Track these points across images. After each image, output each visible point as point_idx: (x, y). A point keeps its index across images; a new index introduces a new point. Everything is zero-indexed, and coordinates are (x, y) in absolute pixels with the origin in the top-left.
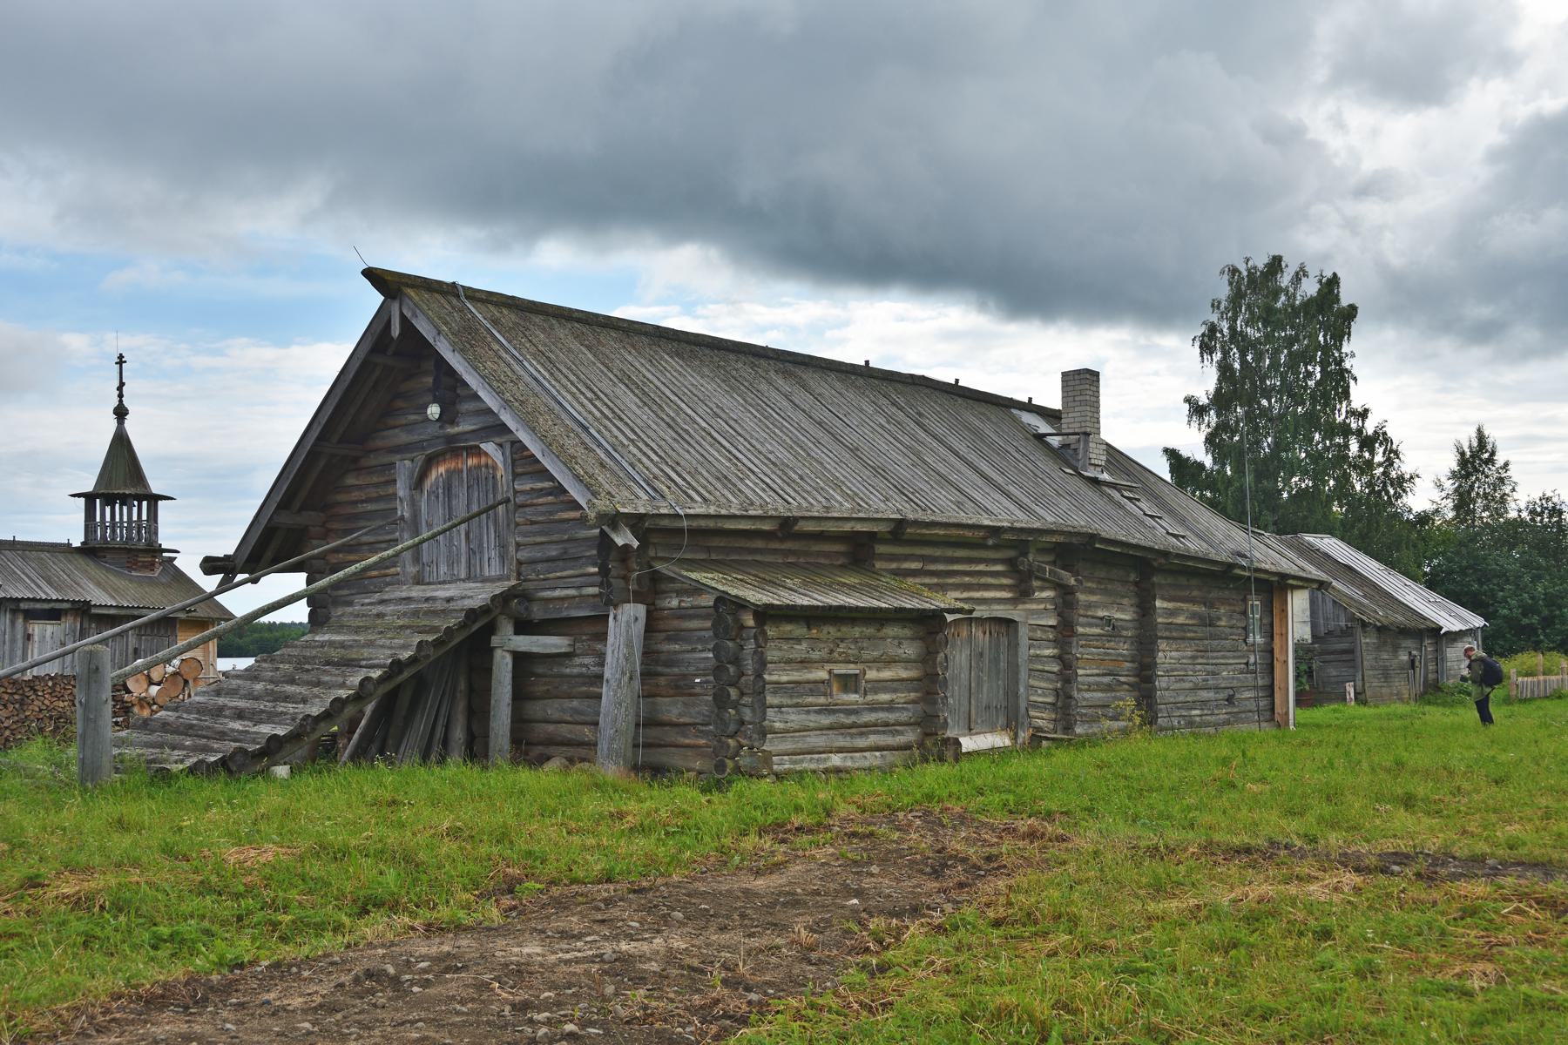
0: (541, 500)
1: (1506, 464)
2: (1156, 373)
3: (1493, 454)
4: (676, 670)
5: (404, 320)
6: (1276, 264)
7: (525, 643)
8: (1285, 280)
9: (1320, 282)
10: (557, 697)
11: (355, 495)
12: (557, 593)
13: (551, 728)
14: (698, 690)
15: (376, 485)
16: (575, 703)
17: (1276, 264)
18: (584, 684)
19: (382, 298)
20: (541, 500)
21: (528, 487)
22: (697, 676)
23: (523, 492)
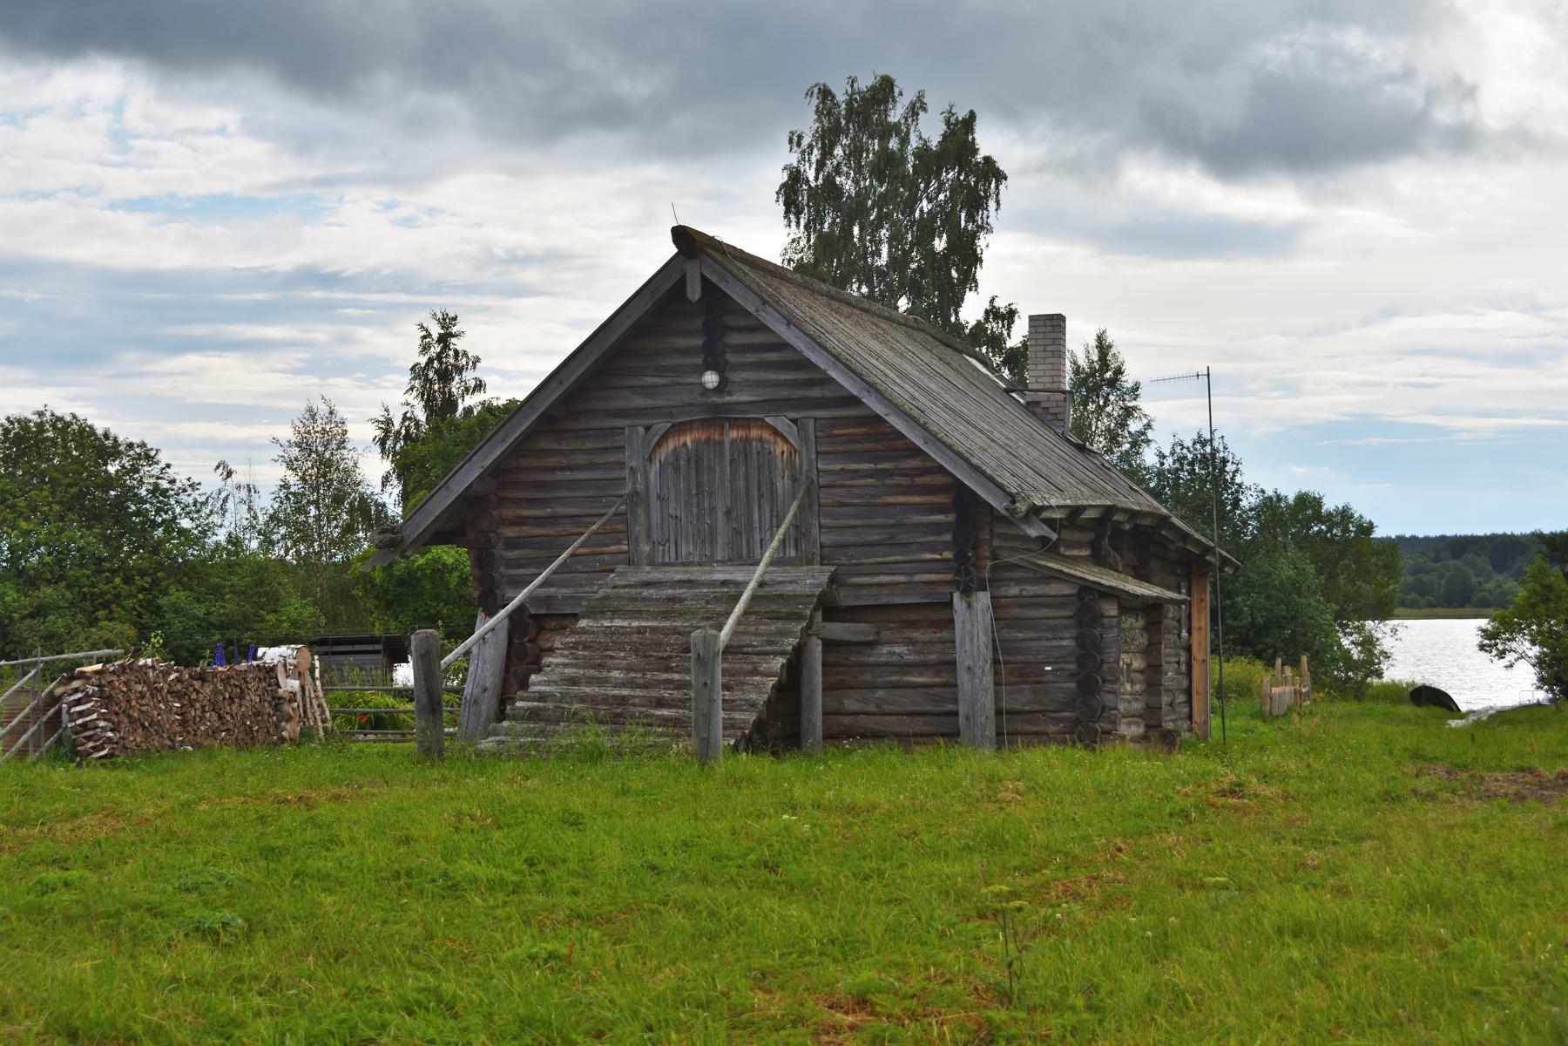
0: (856, 482)
1: (1136, 388)
2: (222, 131)
3: (1119, 371)
4: (1021, 658)
5: (706, 283)
6: (884, 90)
7: (837, 630)
8: (895, 115)
9: (948, 122)
10: (852, 687)
11: (552, 461)
12: (867, 580)
13: (847, 720)
14: (1048, 677)
15: (588, 452)
16: (880, 693)
17: (884, 90)
18: (895, 673)
19: (676, 250)
20: (856, 482)
21: (839, 467)
22: (1048, 664)
23: (827, 472)
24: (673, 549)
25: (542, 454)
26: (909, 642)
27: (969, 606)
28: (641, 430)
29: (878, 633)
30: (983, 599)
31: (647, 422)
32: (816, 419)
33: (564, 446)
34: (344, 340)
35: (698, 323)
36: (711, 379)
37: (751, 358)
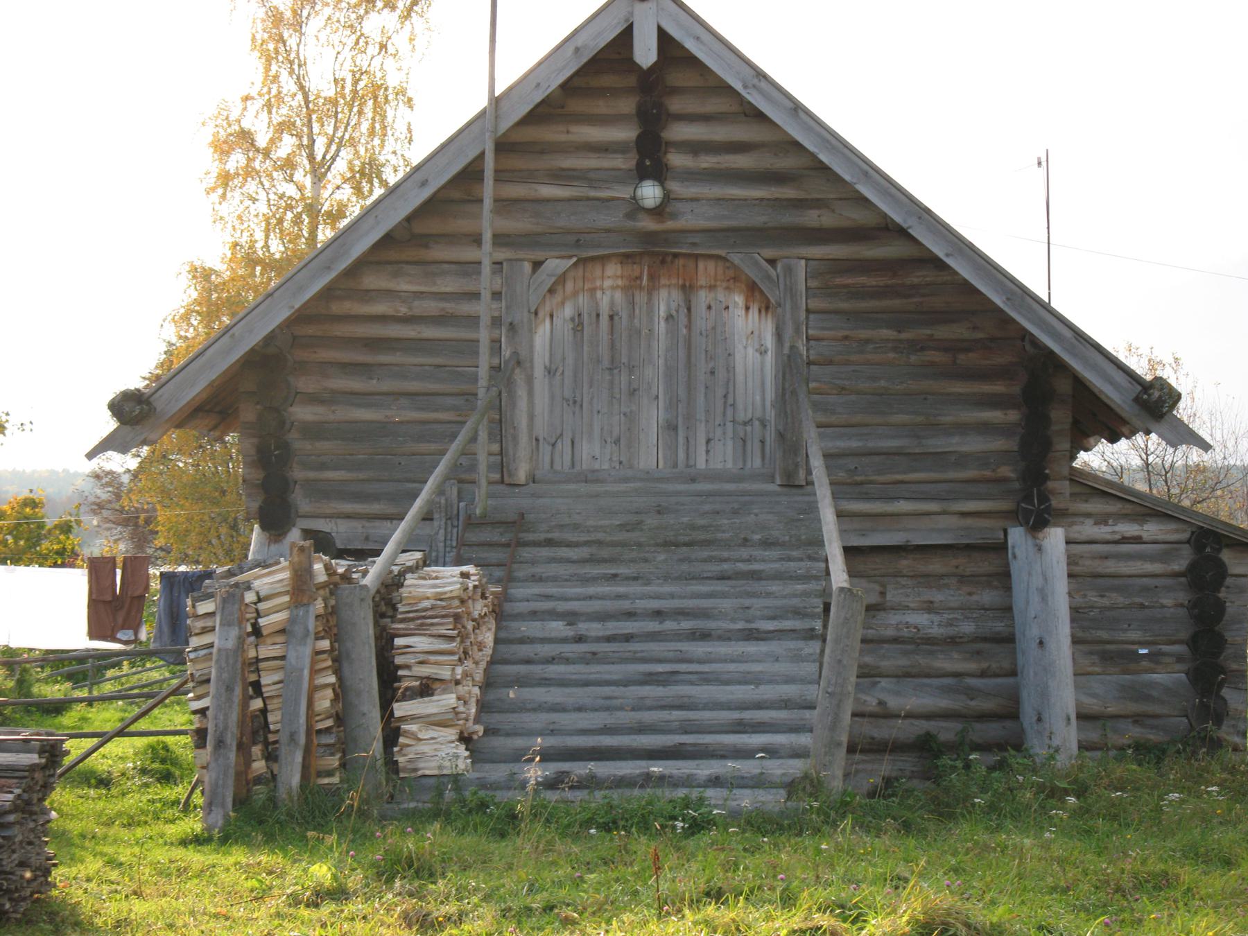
24: (568, 450)
25: (368, 295)
26: (930, 608)
27: (1040, 549)
28: (527, 267)
29: (883, 594)
30: (1055, 537)
31: (538, 255)
32: (807, 259)
33: (404, 286)
34: (950, 624)
35: (627, 105)
36: (650, 193)
37: (707, 162)
